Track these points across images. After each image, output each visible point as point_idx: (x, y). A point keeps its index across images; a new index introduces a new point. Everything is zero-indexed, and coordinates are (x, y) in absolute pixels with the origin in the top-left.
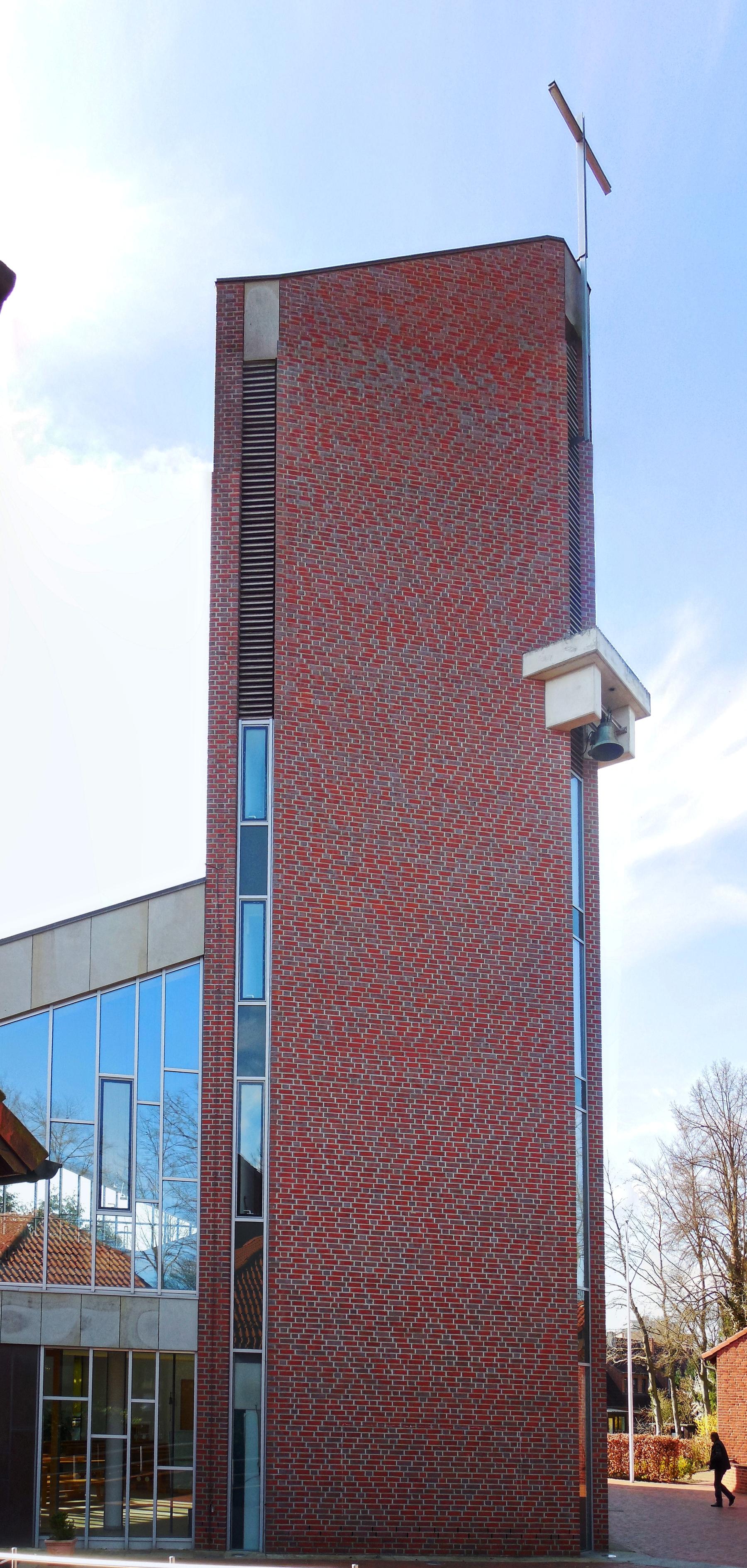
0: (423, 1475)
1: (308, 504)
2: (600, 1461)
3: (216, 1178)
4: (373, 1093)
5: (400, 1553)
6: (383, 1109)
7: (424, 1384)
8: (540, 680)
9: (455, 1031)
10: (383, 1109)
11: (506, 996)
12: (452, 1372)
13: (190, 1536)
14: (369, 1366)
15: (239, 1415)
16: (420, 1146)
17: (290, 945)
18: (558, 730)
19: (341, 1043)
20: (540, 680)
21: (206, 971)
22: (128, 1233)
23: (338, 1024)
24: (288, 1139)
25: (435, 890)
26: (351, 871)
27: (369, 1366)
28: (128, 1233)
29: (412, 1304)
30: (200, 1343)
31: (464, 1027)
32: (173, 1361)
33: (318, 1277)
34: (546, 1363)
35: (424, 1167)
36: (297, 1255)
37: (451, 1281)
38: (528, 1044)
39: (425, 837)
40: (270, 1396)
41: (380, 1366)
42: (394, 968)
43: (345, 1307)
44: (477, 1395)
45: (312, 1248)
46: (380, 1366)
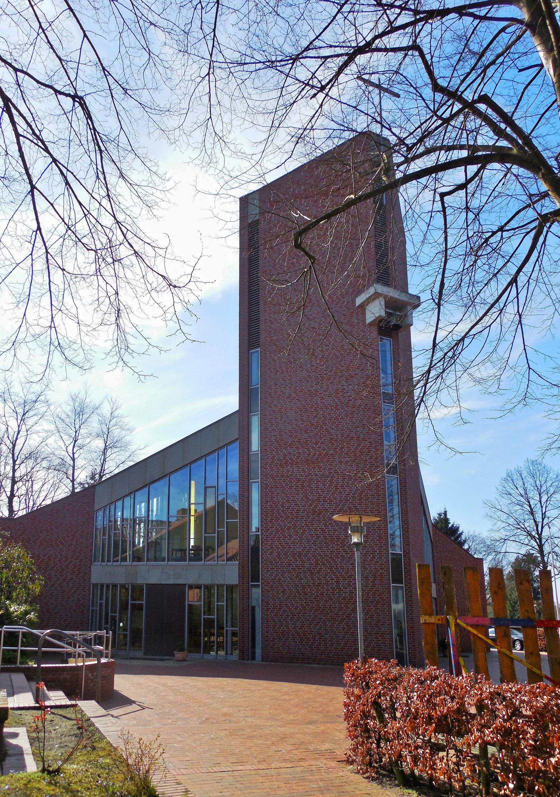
0: (322, 632)
1: (270, 267)
2: (411, 628)
3: (243, 519)
4: (298, 481)
5: (314, 664)
6: (303, 487)
7: (322, 594)
8: (363, 306)
9: (331, 452)
10: (303, 487)
11: (352, 434)
12: (333, 589)
13: (189, 605)
14: (300, 588)
15: (253, 608)
16: (318, 500)
17: (266, 429)
18: (371, 324)
19: (286, 463)
20: (363, 306)
21: (239, 443)
22: (468, 141)
23: (285, 456)
24: (267, 502)
25: (322, 398)
26: (289, 397)
27: (300, 588)
28: (468, 141)
29: (316, 562)
30: (239, 581)
31: (335, 450)
32: (231, 588)
33: (279, 554)
34: (373, 586)
35: (319, 507)
36: (271, 545)
37: (332, 552)
38: (361, 452)
39: (317, 378)
40: (262, 600)
41: (304, 588)
42: (306, 432)
43: (290, 565)
44: (344, 598)
45: (276, 543)
46: (304, 588)
